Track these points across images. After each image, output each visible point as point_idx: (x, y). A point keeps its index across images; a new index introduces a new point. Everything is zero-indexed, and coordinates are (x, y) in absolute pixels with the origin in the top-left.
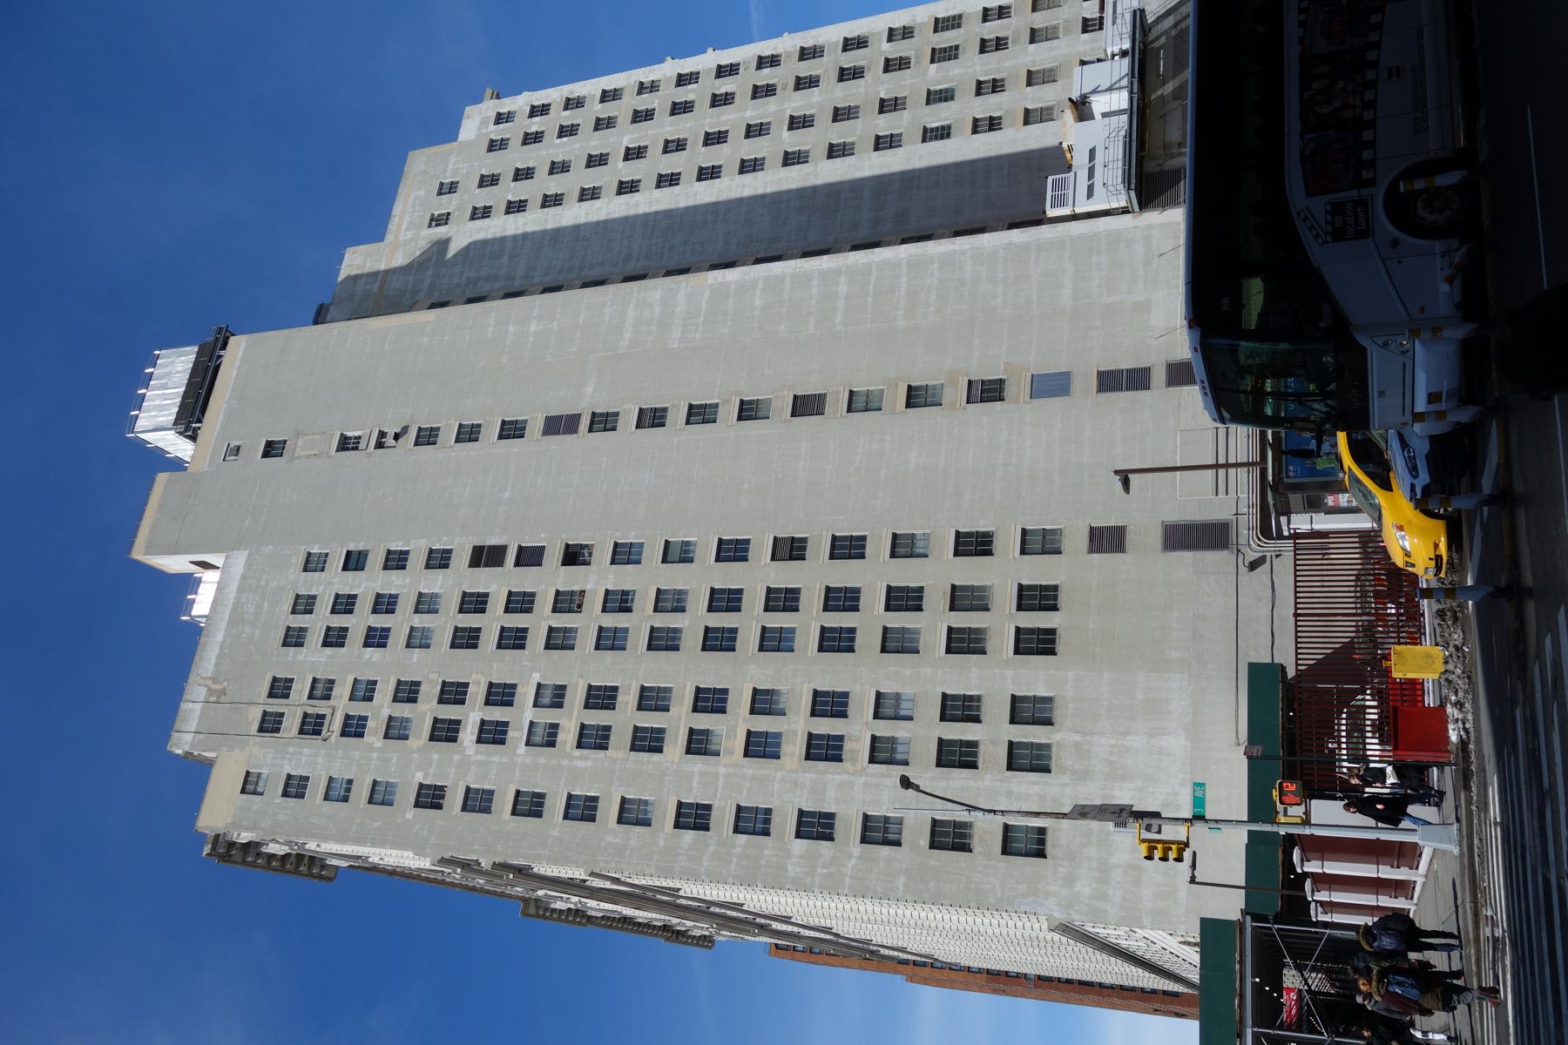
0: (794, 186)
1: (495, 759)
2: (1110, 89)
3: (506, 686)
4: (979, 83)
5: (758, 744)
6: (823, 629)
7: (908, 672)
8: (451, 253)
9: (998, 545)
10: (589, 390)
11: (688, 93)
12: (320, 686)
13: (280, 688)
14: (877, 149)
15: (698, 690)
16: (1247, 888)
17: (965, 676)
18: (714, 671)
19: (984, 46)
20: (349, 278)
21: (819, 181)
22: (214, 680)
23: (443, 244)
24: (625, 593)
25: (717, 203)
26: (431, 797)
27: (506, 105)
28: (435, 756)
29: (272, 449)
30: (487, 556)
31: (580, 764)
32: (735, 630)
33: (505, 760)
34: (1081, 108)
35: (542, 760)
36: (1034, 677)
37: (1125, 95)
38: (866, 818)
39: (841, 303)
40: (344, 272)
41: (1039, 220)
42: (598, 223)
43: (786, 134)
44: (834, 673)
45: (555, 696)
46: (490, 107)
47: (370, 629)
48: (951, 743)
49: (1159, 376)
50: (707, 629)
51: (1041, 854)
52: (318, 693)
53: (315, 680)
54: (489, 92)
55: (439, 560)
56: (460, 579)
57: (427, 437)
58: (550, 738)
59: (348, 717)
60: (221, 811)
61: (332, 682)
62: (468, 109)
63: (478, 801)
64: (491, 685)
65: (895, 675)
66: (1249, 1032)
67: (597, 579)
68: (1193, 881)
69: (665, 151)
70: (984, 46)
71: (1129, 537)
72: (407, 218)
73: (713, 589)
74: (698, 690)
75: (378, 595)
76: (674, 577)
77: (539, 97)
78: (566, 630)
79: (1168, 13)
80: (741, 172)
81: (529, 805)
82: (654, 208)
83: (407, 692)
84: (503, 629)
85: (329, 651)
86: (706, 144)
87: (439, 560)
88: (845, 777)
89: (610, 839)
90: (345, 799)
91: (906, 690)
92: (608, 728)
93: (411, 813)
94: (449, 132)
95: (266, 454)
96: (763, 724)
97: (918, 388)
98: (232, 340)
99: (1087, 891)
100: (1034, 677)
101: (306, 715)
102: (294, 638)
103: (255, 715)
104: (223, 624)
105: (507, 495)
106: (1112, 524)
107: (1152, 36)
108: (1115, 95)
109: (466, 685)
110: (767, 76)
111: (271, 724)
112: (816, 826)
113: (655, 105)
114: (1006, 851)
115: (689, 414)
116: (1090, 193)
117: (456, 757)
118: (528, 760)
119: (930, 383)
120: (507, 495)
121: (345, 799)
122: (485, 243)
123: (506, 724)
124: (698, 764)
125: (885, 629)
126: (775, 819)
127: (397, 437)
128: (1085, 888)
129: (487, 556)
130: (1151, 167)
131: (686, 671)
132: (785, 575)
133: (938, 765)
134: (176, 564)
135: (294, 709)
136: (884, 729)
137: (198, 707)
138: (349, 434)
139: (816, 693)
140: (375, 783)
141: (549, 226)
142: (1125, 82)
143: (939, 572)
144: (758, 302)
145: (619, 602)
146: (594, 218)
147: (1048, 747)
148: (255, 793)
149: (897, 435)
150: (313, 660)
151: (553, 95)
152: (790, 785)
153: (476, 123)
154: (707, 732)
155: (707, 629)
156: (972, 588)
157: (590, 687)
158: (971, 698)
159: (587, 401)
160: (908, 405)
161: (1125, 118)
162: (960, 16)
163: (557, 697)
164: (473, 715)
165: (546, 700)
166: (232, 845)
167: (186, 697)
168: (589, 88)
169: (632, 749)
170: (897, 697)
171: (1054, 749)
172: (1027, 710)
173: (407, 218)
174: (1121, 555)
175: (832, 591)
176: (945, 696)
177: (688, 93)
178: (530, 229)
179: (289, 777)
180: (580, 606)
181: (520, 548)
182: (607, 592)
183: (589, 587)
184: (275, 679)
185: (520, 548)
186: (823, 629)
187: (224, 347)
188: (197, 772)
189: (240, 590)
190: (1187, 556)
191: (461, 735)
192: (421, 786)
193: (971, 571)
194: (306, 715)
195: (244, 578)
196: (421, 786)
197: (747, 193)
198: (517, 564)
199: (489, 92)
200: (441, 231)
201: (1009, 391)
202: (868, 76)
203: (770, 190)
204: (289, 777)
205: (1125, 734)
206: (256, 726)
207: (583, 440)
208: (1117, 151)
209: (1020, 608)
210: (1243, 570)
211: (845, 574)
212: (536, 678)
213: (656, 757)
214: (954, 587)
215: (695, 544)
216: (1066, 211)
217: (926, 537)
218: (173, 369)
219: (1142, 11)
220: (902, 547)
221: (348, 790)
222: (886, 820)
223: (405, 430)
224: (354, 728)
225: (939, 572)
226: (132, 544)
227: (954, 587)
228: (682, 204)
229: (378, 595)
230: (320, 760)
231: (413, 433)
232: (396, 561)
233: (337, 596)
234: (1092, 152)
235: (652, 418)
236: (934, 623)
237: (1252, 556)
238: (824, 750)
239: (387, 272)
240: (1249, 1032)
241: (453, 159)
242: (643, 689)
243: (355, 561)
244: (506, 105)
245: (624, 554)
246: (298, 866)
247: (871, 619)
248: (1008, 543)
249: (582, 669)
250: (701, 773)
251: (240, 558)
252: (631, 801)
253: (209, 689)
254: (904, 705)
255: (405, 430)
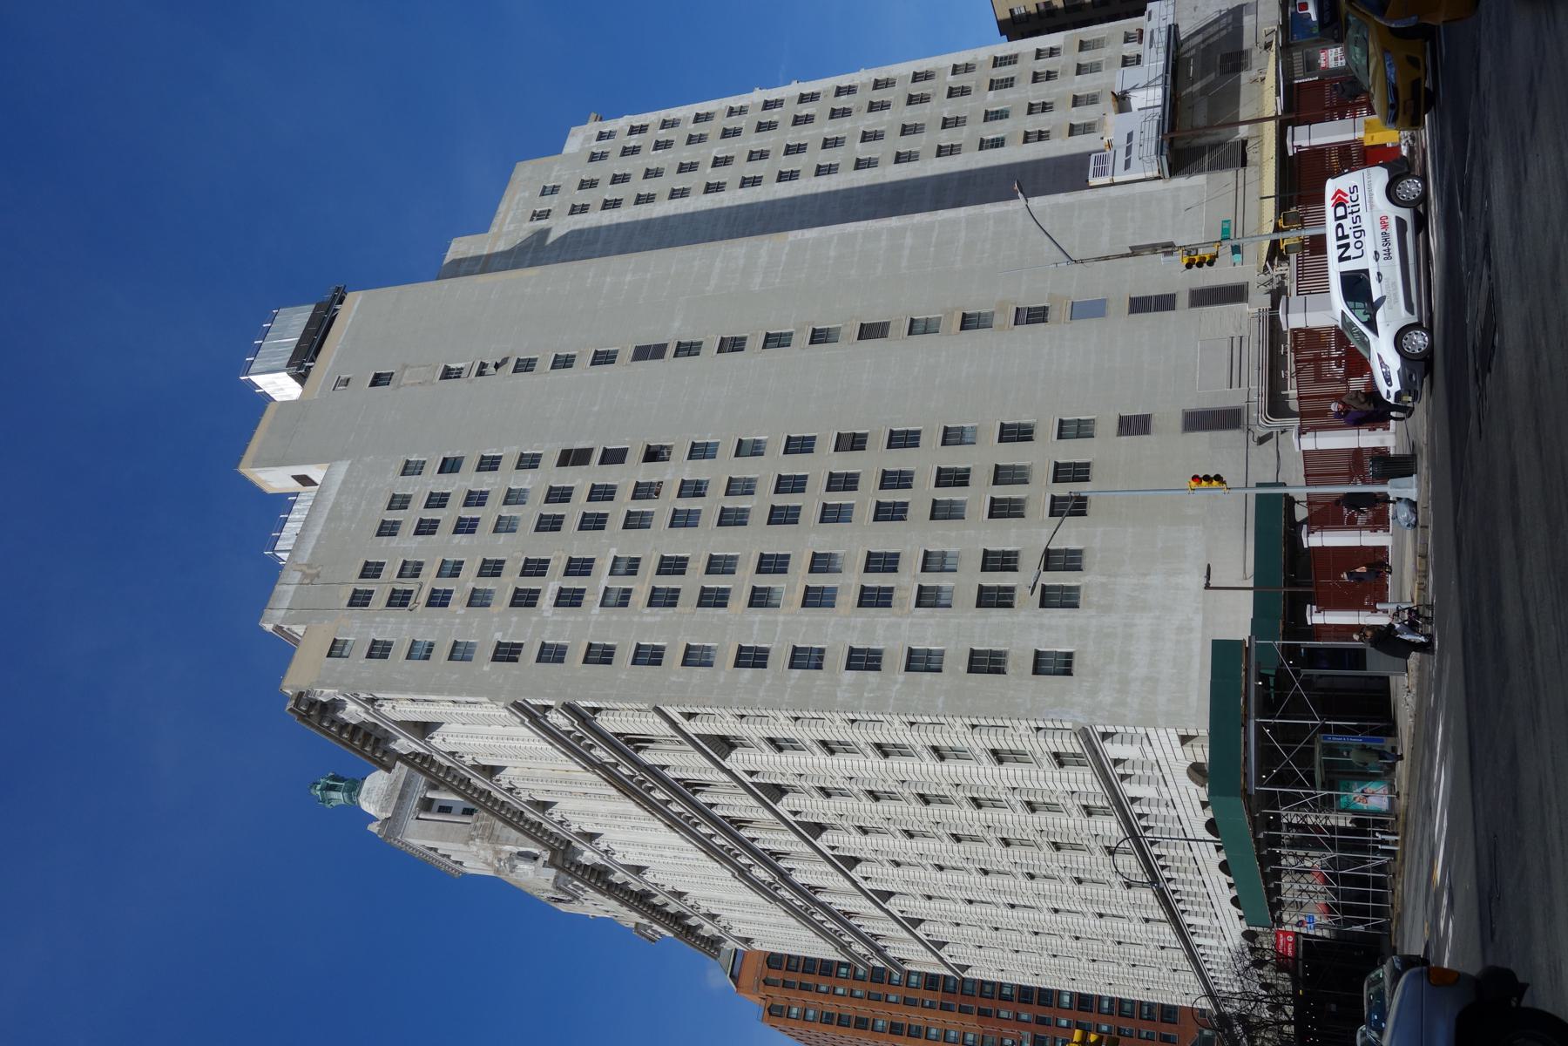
0: (864, 184)
1: (571, 618)
2: (1147, 86)
3: (585, 560)
4: (1031, 105)
5: (815, 597)
6: (879, 504)
7: (953, 534)
8: (550, 240)
9: (1037, 433)
10: (677, 324)
11: (773, 115)
12: (410, 567)
13: (372, 570)
14: (938, 155)
15: (762, 556)
16: (1257, 589)
17: (1005, 535)
18: (777, 540)
19: (1036, 78)
20: (454, 261)
21: (887, 180)
22: (309, 566)
23: (545, 233)
24: (698, 482)
25: (794, 198)
26: (507, 653)
27: (608, 126)
28: (515, 619)
29: (378, 380)
30: (572, 458)
31: (649, 619)
32: (799, 508)
33: (580, 619)
34: (1122, 102)
35: (615, 618)
36: (1070, 535)
37: (1159, 91)
38: (911, 651)
39: (906, 252)
40: (447, 261)
41: (1084, 185)
42: (685, 215)
43: (858, 145)
44: (886, 538)
45: (630, 566)
46: (593, 127)
47: (460, 519)
48: (989, 589)
49: (1183, 300)
50: (773, 507)
51: (1068, 673)
52: (407, 572)
53: (405, 563)
54: (593, 115)
55: (529, 462)
56: (551, 475)
57: (525, 366)
58: (624, 598)
59: (434, 591)
60: (307, 675)
61: (421, 564)
62: (573, 129)
63: (552, 654)
64: (571, 559)
65: (943, 537)
66: (1252, 723)
67: (671, 474)
68: (1207, 587)
69: (750, 160)
70: (1036, 78)
71: (1154, 422)
72: (511, 214)
73: (780, 477)
74: (762, 556)
75: (470, 492)
76: (746, 468)
77: (637, 120)
78: (643, 513)
79: (1198, 32)
80: (817, 175)
81: (600, 655)
82: (737, 203)
83: (492, 568)
84: (585, 515)
85: (420, 538)
86: (786, 153)
87: (529, 462)
88: (893, 619)
89: (673, 679)
90: (427, 658)
91: (950, 549)
92: (678, 590)
93: (488, 667)
94: (554, 146)
95: (373, 384)
96: (820, 580)
97: (971, 316)
98: (350, 297)
99: (1109, 700)
100: (1070, 535)
101: (394, 591)
102: (388, 529)
103: (347, 594)
104: (322, 521)
105: (596, 408)
106: (1139, 412)
107: (1183, 50)
108: (1151, 91)
109: (548, 561)
110: (843, 102)
111: (360, 599)
112: (864, 660)
113: (743, 125)
114: (1036, 671)
115: (766, 341)
116: (1127, 165)
117: (535, 619)
118: (602, 618)
119: (983, 311)
120: (596, 408)
121: (427, 658)
122: (581, 232)
123: (583, 591)
124: (759, 614)
125: (935, 502)
126: (828, 656)
127: (497, 366)
128: (1106, 697)
129: (572, 458)
130: (1179, 144)
131: (748, 544)
132: (846, 463)
133: (979, 605)
134: (275, 480)
135: (381, 589)
136: (930, 580)
137: (292, 588)
138: (452, 366)
139: (870, 554)
140: (456, 643)
141: (641, 218)
142: (1160, 81)
143: (982, 457)
144: (832, 253)
145: (693, 489)
146: (682, 211)
147: (1077, 589)
148: (340, 656)
149: (953, 346)
150: (407, 545)
151: (652, 118)
152: (841, 628)
153: (579, 140)
154: (768, 590)
155: (773, 507)
156: (1013, 468)
157: (663, 558)
158: (1009, 553)
159: (674, 332)
160: (962, 328)
161: (1159, 110)
162: (1016, 56)
163: (633, 567)
164: (551, 585)
165: (622, 570)
166: (313, 704)
167: (270, 604)
168: (685, 112)
169: (699, 605)
170: (944, 554)
171: (1082, 591)
172: (1069, 560)
173: (511, 214)
174: (1145, 437)
175: (890, 474)
176: (986, 552)
177: (773, 115)
178: (623, 220)
179: (374, 642)
180: (657, 494)
181: (605, 450)
182: (683, 482)
183: (666, 478)
184: (367, 563)
185: (605, 450)
186: (879, 504)
187: (341, 302)
188: (283, 649)
189: (340, 493)
190: (1204, 436)
191: (539, 601)
192: (499, 644)
193: (1013, 454)
194: (394, 591)
195: (344, 482)
196: (499, 644)
197: (822, 189)
198: (602, 462)
199: (593, 115)
200: (543, 224)
201: (1052, 315)
202: (934, 102)
203: (841, 187)
204: (374, 642)
205: (1145, 575)
206: (347, 601)
207: (669, 362)
208: (1152, 131)
209: (1055, 480)
210: (1251, 443)
211: (899, 460)
212: (614, 552)
213: (721, 611)
214: (997, 467)
215: (765, 442)
216: (1106, 180)
217: (956, 556)
218: (292, 323)
219: (1176, 26)
220: (951, 437)
221: (430, 651)
222: (929, 652)
223: (505, 361)
224: (439, 599)
225: (982, 457)
226: (240, 460)
227: (997, 467)
228: (763, 199)
229: (470, 492)
230: (405, 627)
231: (512, 364)
232: (489, 464)
233: (432, 494)
234: (1130, 136)
235: (733, 345)
236: (977, 496)
237: (1263, 432)
238: (874, 599)
239: (489, 256)
240: (1252, 723)
241: (556, 168)
242: (711, 557)
243: (450, 466)
244: (608, 126)
245: (699, 451)
246: (364, 745)
247: (922, 494)
248: (1047, 431)
249: (654, 544)
250: (761, 622)
251: (342, 468)
252: (694, 648)
253: (304, 574)
254: (948, 561)
255: (505, 361)
